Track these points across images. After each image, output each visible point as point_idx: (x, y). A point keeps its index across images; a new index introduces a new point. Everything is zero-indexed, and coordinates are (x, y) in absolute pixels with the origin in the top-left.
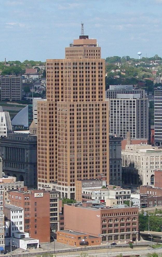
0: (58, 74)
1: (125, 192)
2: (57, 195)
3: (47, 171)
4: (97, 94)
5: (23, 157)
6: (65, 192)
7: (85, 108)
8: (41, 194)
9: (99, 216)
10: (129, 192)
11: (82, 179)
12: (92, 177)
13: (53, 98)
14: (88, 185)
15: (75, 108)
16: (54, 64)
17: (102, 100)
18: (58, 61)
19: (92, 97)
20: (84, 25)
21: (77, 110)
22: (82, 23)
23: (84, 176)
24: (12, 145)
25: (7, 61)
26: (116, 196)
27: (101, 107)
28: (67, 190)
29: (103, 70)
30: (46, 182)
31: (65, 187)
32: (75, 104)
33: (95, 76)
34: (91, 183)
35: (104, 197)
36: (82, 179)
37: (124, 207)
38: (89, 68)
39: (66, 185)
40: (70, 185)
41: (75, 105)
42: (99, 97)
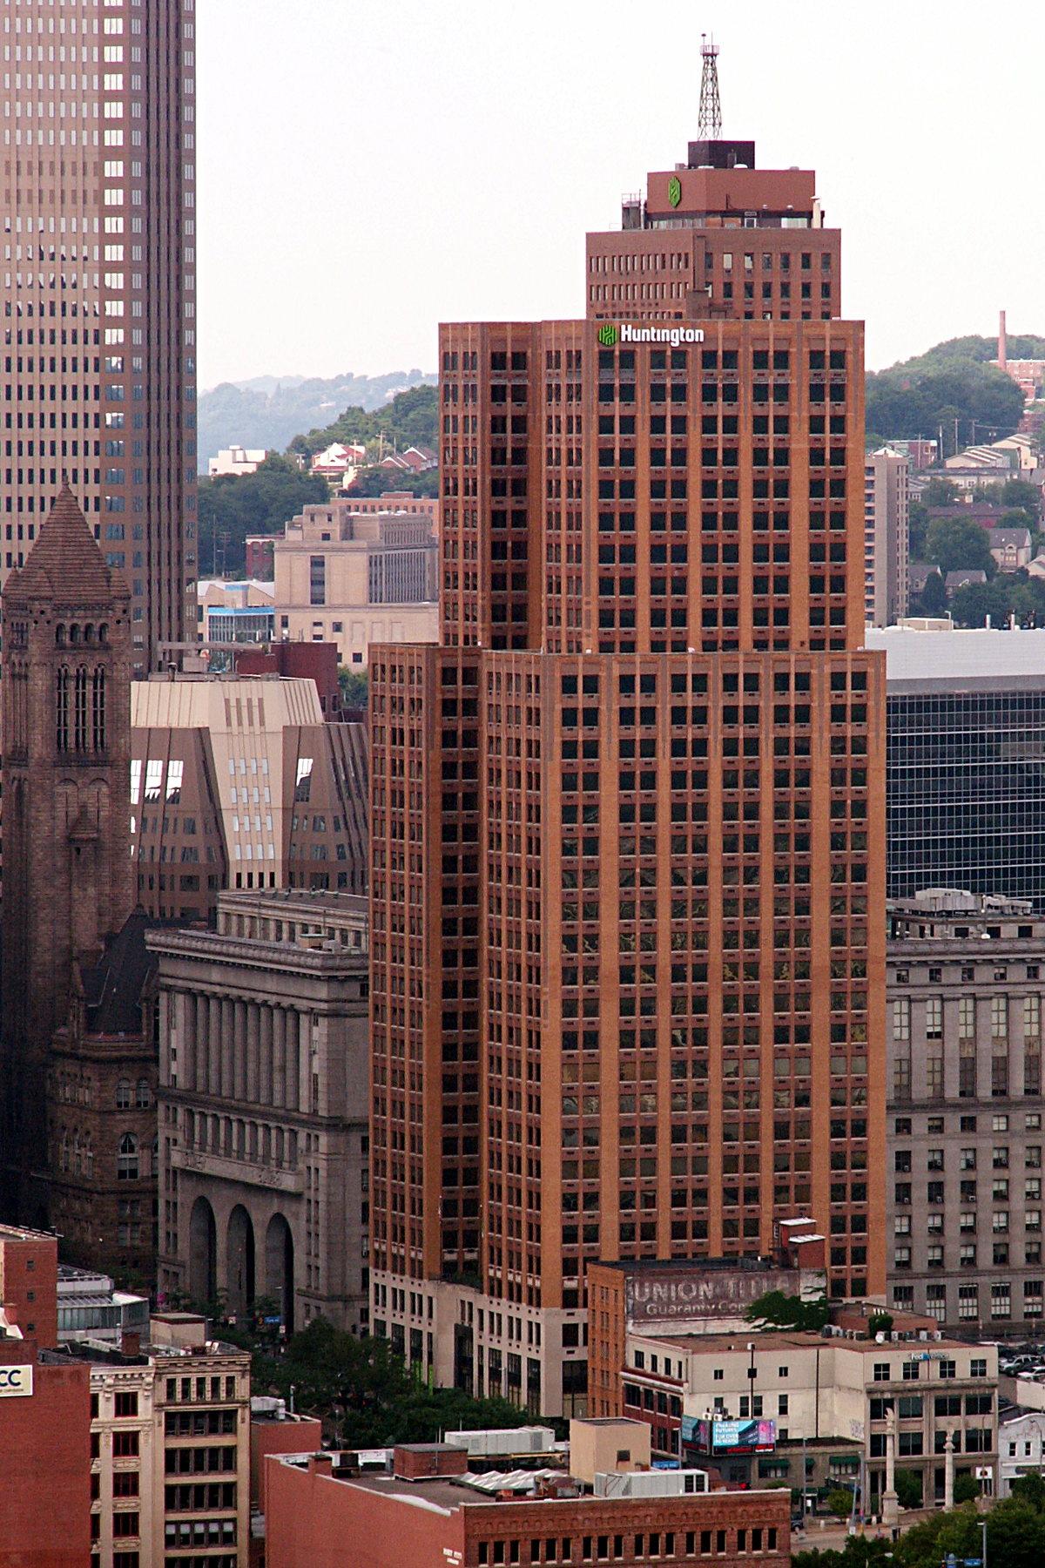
0: (515, 440)
1: (948, 1368)
2: (230, 1380)
3: (424, 1187)
4: (800, 598)
5: (290, 1073)
6: (525, 1352)
7: (638, 705)
8: (15, 1378)
9: (458, 1555)
10: (983, 1362)
11: (664, 1254)
12: (689, 1243)
13: (479, 624)
14: (679, 1301)
15: (609, 702)
16: (483, 361)
17: (839, 644)
18: (515, 340)
19: (759, 617)
20: (719, 61)
21: (626, 716)
22: (708, 41)
23: (678, 1230)
24: (205, 977)
25: (1015, 330)
26: (869, 1392)
27: (821, 700)
28: (538, 1343)
29: (789, 408)
30: (417, 1272)
31: (524, 1313)
32: (612, 669)
33: (783, 456)
34: (703, 1287)
35: (784, 1399)
36: (664, 1254)
37: (682, 1493)
38: (731, 393)
39: (535, 1298)
40: (560, 1301)
41: (610, 676)
42: (816, 617)
